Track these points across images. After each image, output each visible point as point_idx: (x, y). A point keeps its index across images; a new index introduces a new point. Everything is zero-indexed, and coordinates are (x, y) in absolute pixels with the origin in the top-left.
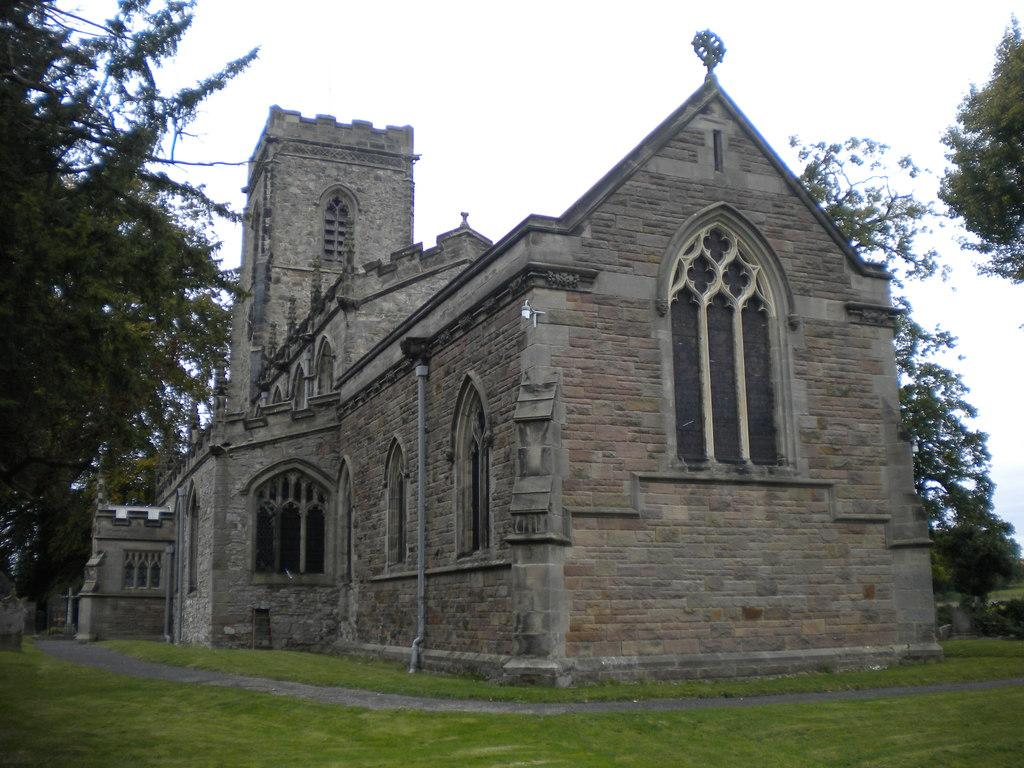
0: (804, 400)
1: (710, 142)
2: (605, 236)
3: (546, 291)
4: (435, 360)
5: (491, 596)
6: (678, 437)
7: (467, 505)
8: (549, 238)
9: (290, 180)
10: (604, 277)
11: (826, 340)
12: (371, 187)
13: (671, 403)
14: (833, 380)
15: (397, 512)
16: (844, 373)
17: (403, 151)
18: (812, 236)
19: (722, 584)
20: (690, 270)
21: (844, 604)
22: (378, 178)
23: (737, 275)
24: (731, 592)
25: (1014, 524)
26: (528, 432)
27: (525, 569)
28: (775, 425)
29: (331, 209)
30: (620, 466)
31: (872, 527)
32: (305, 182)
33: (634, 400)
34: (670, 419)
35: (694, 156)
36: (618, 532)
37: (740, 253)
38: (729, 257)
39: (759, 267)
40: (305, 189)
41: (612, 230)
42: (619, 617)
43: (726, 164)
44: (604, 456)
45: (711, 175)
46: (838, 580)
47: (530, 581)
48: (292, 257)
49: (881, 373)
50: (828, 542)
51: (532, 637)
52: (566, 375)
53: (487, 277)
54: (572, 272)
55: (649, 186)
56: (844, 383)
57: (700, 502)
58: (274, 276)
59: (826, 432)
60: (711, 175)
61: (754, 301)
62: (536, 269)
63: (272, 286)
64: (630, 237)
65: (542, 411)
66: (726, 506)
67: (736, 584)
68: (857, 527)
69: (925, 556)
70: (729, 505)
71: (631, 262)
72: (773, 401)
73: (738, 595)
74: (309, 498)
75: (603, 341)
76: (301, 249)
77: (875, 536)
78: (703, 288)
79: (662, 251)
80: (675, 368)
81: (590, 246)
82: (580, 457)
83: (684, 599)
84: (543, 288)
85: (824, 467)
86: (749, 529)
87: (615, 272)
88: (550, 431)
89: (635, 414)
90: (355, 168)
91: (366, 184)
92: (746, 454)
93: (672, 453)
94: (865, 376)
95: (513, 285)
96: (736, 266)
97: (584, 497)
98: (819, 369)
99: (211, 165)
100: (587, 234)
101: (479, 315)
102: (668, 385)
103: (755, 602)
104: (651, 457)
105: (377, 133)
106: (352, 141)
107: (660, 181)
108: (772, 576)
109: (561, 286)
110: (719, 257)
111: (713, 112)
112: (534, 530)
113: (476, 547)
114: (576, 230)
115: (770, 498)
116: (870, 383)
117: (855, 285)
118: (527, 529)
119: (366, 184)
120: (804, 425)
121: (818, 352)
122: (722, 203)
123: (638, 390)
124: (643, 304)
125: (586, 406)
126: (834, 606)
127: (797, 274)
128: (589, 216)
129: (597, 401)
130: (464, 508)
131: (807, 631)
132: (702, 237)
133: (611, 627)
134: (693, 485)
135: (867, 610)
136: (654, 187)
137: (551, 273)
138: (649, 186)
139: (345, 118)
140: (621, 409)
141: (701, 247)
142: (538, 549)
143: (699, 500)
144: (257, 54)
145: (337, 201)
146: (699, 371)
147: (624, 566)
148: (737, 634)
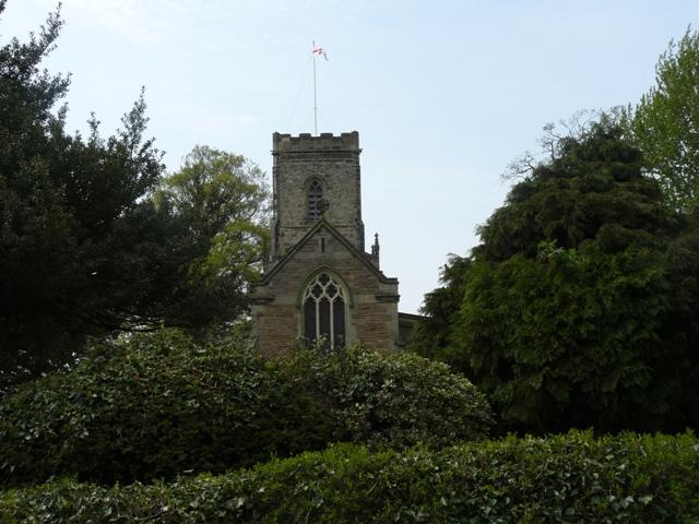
9: (286, 176)
12: (334, 172)
17: (353, 148)
22: (337, 167)
23: (332, 290)
29: (312, 188)
32: (298, 175)
40: (295, 180)
43: (326, 249)
63: (280, 238)
76: (294, 215)
90: (324, 163)
91: (330, 171)
98: (362, 322)
100: (271, 284)
105: (336, 139)
106: (321, 147)
109: (261, 304)
117: (381, 288)
119: (330, 171)
124: (291, 306)
139: (315, 134)
145: (315, 183)
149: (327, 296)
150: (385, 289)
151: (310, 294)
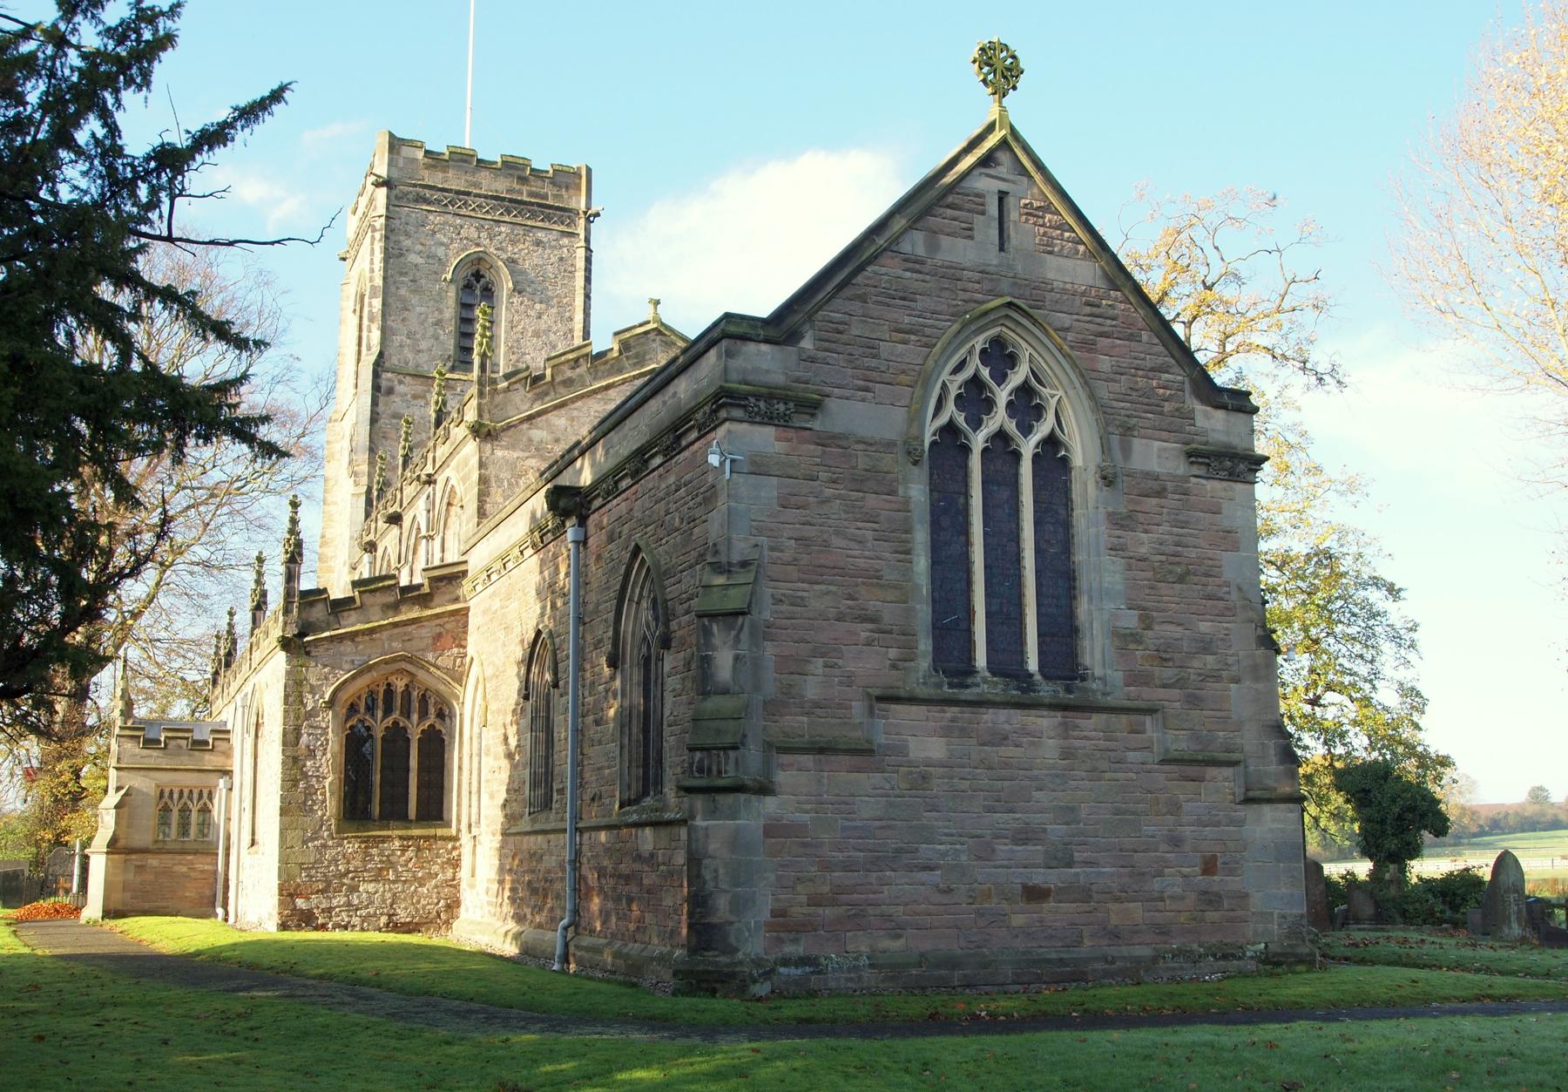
0: (1119, 587)
1: (993, 209)
2: (833, 346)
3: (745, 426)
4: (593, 520)
5: (664, 864)
6: (934, 638)
7: (635, 730)
8: (751, 347)
10: (832, 404)
11: (1154, 501)
13: (925, 590)
14: (1163, 558)
15: (542, 736)
16: (1180, 549)
18: (1141, 349)
19: (994, 851)
20: (959, 397)
21: (1171, 883)
22: (538, 243)
23: (1027, 405)
24: (1005, 863)
25: (1454, 757)
26: (715, 628)
27: (706, 828)
28: (1078, 623)
29: (468, 287)
30: (849, 680)
31: (1211, 772)
33: (872, 585)
34: (923, 613)
35: (970, 229)
36: (843, 776)
37: (1033, 371)
38: (1016, 378)
39: (1060, 393)
41: (844, 337)
42: (844, 897)
44: (826, 666)
45: (993, 257)
46: (1163, 847)
47: (713, 847)
48: (410, 356)
49: (1235, 548)
50: (1150, 792)
51: (714, 926)
52: (772, 549)
53: (664, 403)
54: (785, 400)
55: (900, 272)
56: (1179, 563)
57: (964, 733)
58: (384, 384)
59: (1150, 633)
60: (993, 257)
61: (1052, 443)
62: (730, 394)
63: (382, 400)
64: (871, 347)
65: (735, 600)
66: (1002, 739)
67: (1013, 851)
68: (1192, 771)
69: (1291, 815)
70: (1006, 738)
71: (871, 384)
72: (1074, 588)
73: (1017, 867)
74: (424, 714)
75: (828, 500)
76: (424, 345)
77: (1223, 782)
78: (976, 424)
79: (917, 368)
80: (932, 540)
81: (813, 360)
82: (793, 666)
83: (938, 872)
84: (741, 421)
85: (1146, 684)
86: (1035, 772)
87: (847, 398)
88: (746, 629)
89: (873, 605)
92: (1033, 664)
93: (924, 664)
94: (1210, 553)
95: (699, 416)
96: (1025, 391)
97: (796, 723)
98: (1143, 542)
99: (231, 244)
100: (807, 343)
101: (653, 456)
102: (922, 563)
103: (1039, 877)
104: (894, 667)
106: (501, 186)
107: (917, 266)
108: (1067, 840)
109: (769, 419)
110: (1001, 378)
111: (998, 164)
112: (719, 772)
113: (645, 793)
114: (792, 338)
115: (1065, 731)
116: (1217, 563)
117: (1200, 422)
118: (710, 770)
120: (1119, 624)
121: (1141, 518)
122: (1009, 299)
123: (878, 571)
124: (890, 445)
125: (800, 594)
126: (1157, 884)
127: (1115, 404)
128: (810, 317)
129: (816, 587)
130: (630, 735)
131: (1114, 920)
132: (978, 348)
133: (828, 912)
134: (956, 709)
135: (1206, 893)
136: (908, 274)
137: (752, 400)
138: (900, 272)
140: (851, 598)
141: (975, 363)
142: (726, 800)
143: (963, 730)
144: (287, 95)
146: (968, 544)
147: (850, 823)
148: (1014, 923)
149: (1011, 427)
150: (1213, 424)
151: (950, 408)
